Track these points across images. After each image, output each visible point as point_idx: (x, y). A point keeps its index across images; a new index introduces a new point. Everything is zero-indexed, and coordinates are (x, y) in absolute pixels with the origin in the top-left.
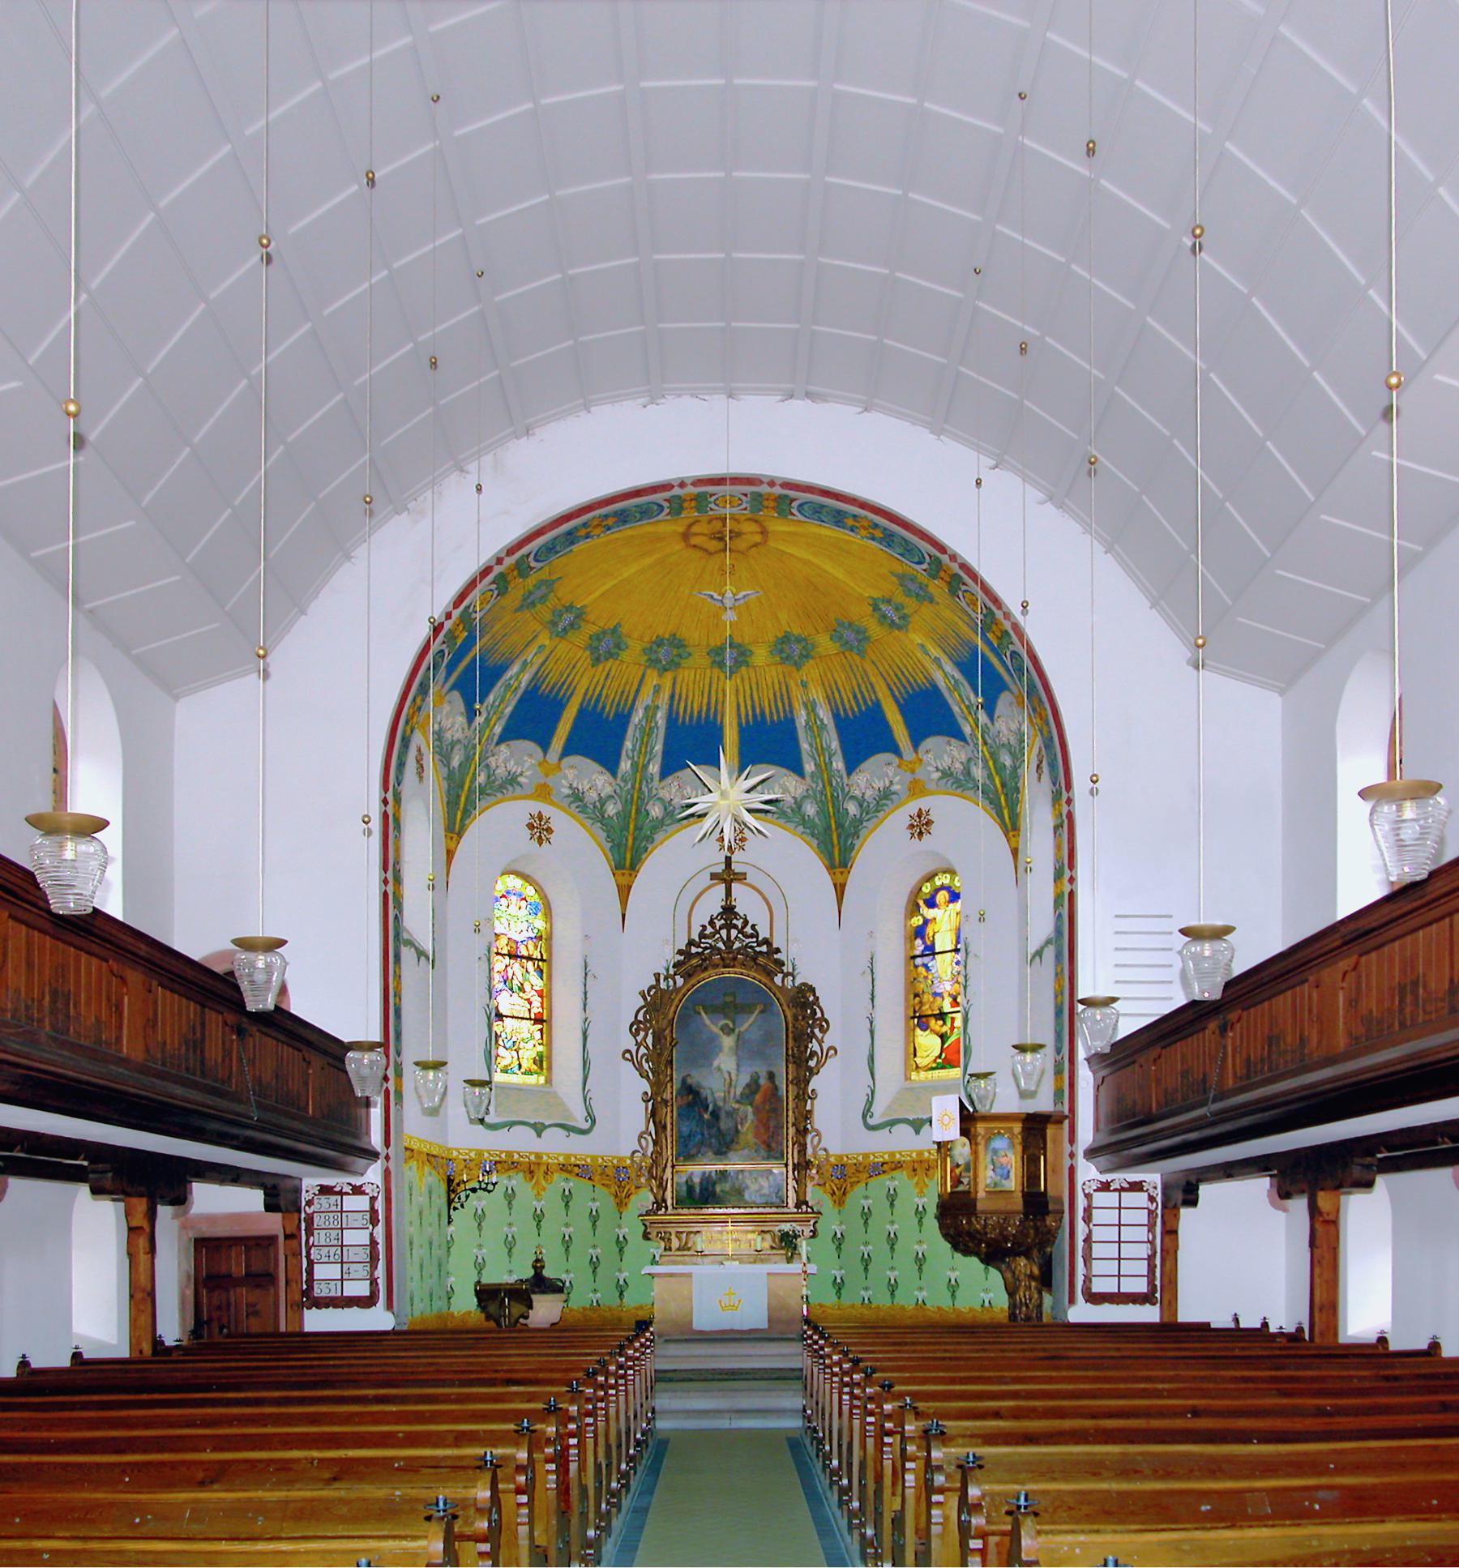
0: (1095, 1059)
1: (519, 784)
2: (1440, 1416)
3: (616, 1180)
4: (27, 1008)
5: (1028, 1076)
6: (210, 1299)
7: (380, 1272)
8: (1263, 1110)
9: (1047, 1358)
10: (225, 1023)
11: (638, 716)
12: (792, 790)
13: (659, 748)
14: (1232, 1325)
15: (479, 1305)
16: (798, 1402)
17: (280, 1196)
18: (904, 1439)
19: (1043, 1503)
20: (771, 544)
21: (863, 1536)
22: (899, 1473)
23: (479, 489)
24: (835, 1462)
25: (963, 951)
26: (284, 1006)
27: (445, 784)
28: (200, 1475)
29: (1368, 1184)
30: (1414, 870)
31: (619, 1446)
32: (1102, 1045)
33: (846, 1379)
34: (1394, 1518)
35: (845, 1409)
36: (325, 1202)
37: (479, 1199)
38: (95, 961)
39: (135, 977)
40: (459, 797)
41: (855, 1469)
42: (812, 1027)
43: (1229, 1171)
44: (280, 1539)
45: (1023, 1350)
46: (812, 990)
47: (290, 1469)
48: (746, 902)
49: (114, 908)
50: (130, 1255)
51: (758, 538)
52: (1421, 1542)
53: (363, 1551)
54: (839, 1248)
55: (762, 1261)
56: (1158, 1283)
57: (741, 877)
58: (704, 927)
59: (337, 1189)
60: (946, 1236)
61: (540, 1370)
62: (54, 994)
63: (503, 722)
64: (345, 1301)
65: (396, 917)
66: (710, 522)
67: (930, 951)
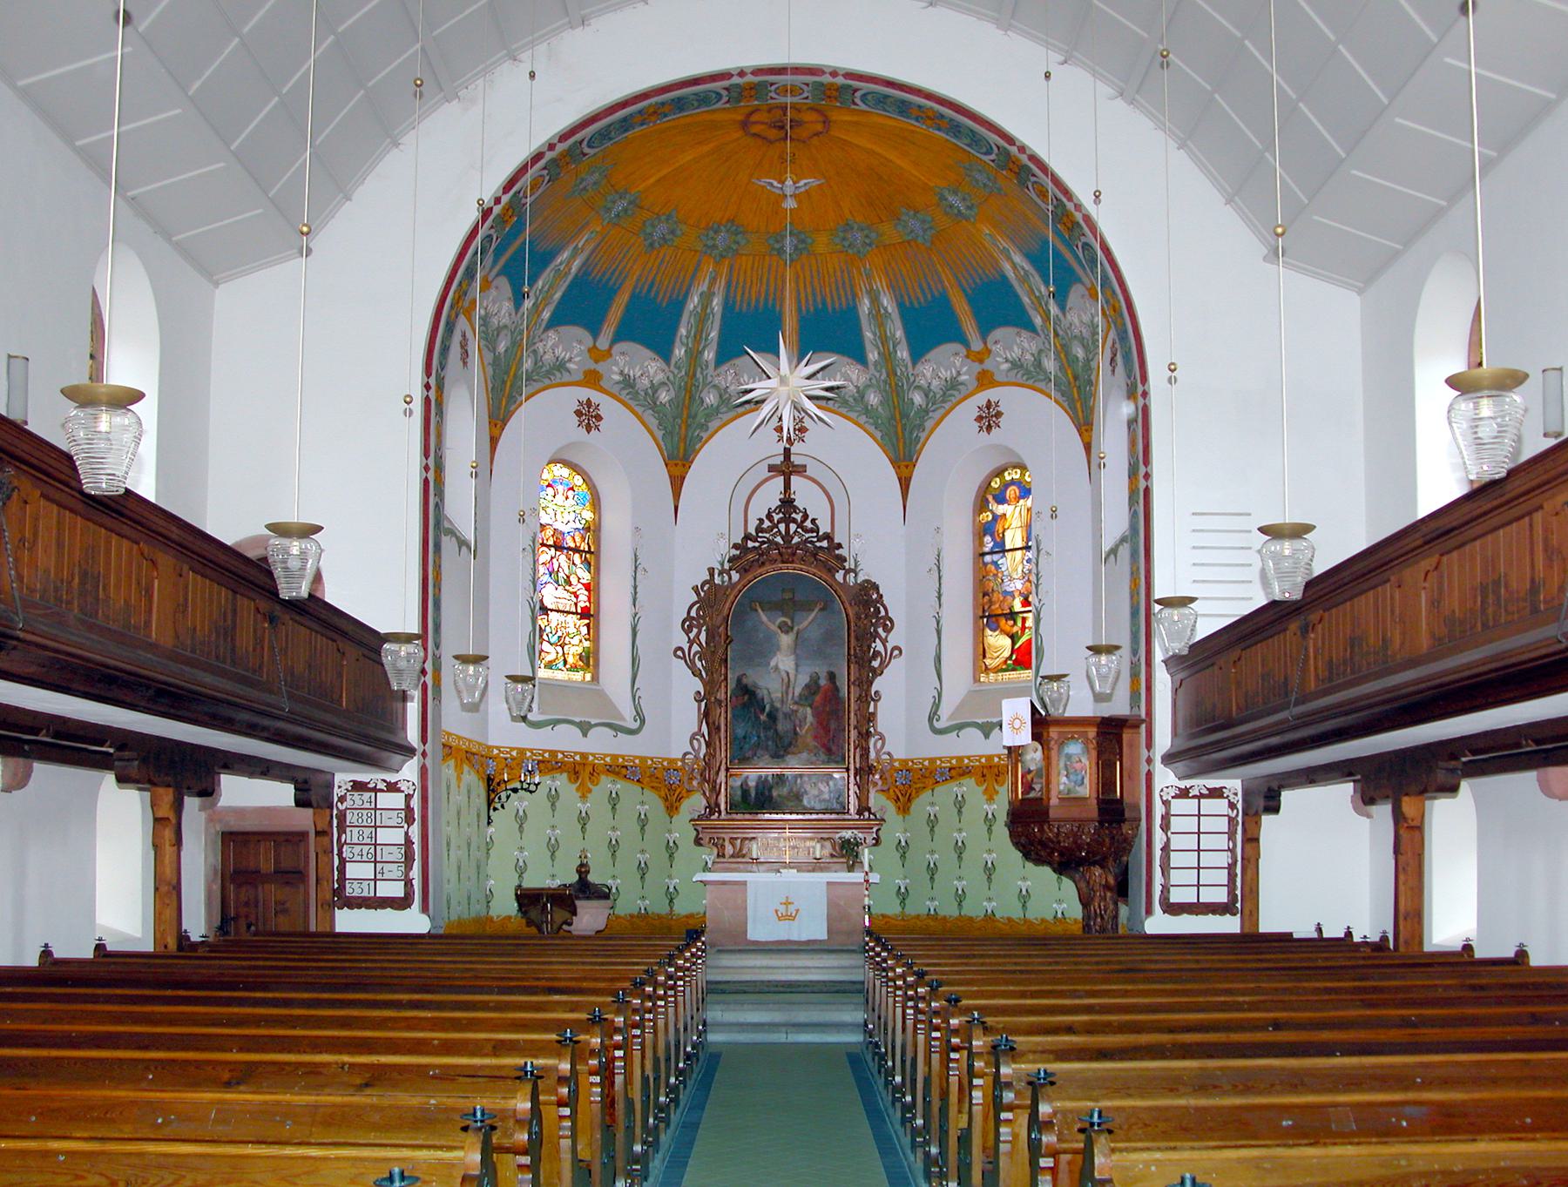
0: (1172, 662)
1: (568, 371)
2: (1531, 1029)
3: (665, 782)
4: (56, 590)
5: (1103, 678)
6: (237, 895)
7: (415, 873)
8: (1346, 714)
9: (1121, 971)
10: (257, 610)
11: (694, 302)
12: (854, 377)
13: (714, 334)
14: (1315, 935)
15: (520, 909)
16: (859, 1016)
17: (311, 792)
18: (971, 1056)
19: (1118, 1120)
20: (834, 132)
21: (927, 1154)
22: (966, 1090)
23: (532, 75)
24: (898, 1079)
25: (1034, 548)
26: (318, 595)
27: (490, 370)
28: (226, 1076)
29: (1453, 789)
30: (1492, 468)
31: (668, 1059)
32: (1179, 647)
33: (910, 993)
34: (1486, 1137)
35: (909, 1023)
36: (357, 799)
37: (521, 800)
38: (126, 544)
39: (166, 560)
40: (504, 382)
41: (920, 1085)
42: (876, 626)
43: (1311, 776)
44: (309, 1144)
45: (1097, 963)
46: (876, 587)
47: (320, 1073)
48: (805, 495)
49: (147, 488)
50: (155, 846)
51: (819, 127)
52: (1516, 1164)
53: (397, 1159)
54: (903, 856)
55: (822, 870)
56: (1238, 892)
57: (801, 470)
58: (761, 521)
59: (371, 785)
60: (1017, 844)
61: (585, 979)
62: (84, 575)
63: (552, 307)
64: (378, 899)
65: (437, 505)
66: (769, 111)
67: (1001, 549)
